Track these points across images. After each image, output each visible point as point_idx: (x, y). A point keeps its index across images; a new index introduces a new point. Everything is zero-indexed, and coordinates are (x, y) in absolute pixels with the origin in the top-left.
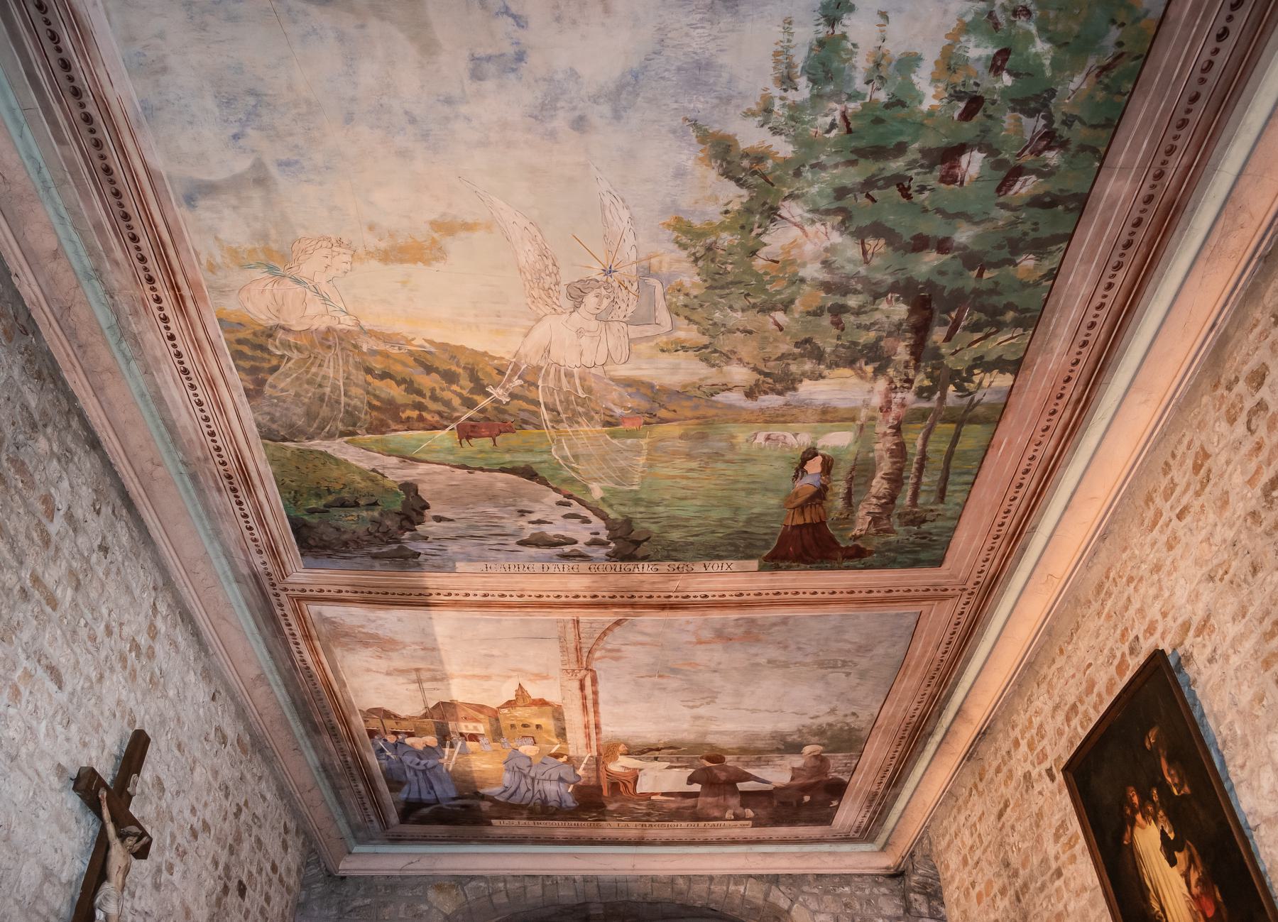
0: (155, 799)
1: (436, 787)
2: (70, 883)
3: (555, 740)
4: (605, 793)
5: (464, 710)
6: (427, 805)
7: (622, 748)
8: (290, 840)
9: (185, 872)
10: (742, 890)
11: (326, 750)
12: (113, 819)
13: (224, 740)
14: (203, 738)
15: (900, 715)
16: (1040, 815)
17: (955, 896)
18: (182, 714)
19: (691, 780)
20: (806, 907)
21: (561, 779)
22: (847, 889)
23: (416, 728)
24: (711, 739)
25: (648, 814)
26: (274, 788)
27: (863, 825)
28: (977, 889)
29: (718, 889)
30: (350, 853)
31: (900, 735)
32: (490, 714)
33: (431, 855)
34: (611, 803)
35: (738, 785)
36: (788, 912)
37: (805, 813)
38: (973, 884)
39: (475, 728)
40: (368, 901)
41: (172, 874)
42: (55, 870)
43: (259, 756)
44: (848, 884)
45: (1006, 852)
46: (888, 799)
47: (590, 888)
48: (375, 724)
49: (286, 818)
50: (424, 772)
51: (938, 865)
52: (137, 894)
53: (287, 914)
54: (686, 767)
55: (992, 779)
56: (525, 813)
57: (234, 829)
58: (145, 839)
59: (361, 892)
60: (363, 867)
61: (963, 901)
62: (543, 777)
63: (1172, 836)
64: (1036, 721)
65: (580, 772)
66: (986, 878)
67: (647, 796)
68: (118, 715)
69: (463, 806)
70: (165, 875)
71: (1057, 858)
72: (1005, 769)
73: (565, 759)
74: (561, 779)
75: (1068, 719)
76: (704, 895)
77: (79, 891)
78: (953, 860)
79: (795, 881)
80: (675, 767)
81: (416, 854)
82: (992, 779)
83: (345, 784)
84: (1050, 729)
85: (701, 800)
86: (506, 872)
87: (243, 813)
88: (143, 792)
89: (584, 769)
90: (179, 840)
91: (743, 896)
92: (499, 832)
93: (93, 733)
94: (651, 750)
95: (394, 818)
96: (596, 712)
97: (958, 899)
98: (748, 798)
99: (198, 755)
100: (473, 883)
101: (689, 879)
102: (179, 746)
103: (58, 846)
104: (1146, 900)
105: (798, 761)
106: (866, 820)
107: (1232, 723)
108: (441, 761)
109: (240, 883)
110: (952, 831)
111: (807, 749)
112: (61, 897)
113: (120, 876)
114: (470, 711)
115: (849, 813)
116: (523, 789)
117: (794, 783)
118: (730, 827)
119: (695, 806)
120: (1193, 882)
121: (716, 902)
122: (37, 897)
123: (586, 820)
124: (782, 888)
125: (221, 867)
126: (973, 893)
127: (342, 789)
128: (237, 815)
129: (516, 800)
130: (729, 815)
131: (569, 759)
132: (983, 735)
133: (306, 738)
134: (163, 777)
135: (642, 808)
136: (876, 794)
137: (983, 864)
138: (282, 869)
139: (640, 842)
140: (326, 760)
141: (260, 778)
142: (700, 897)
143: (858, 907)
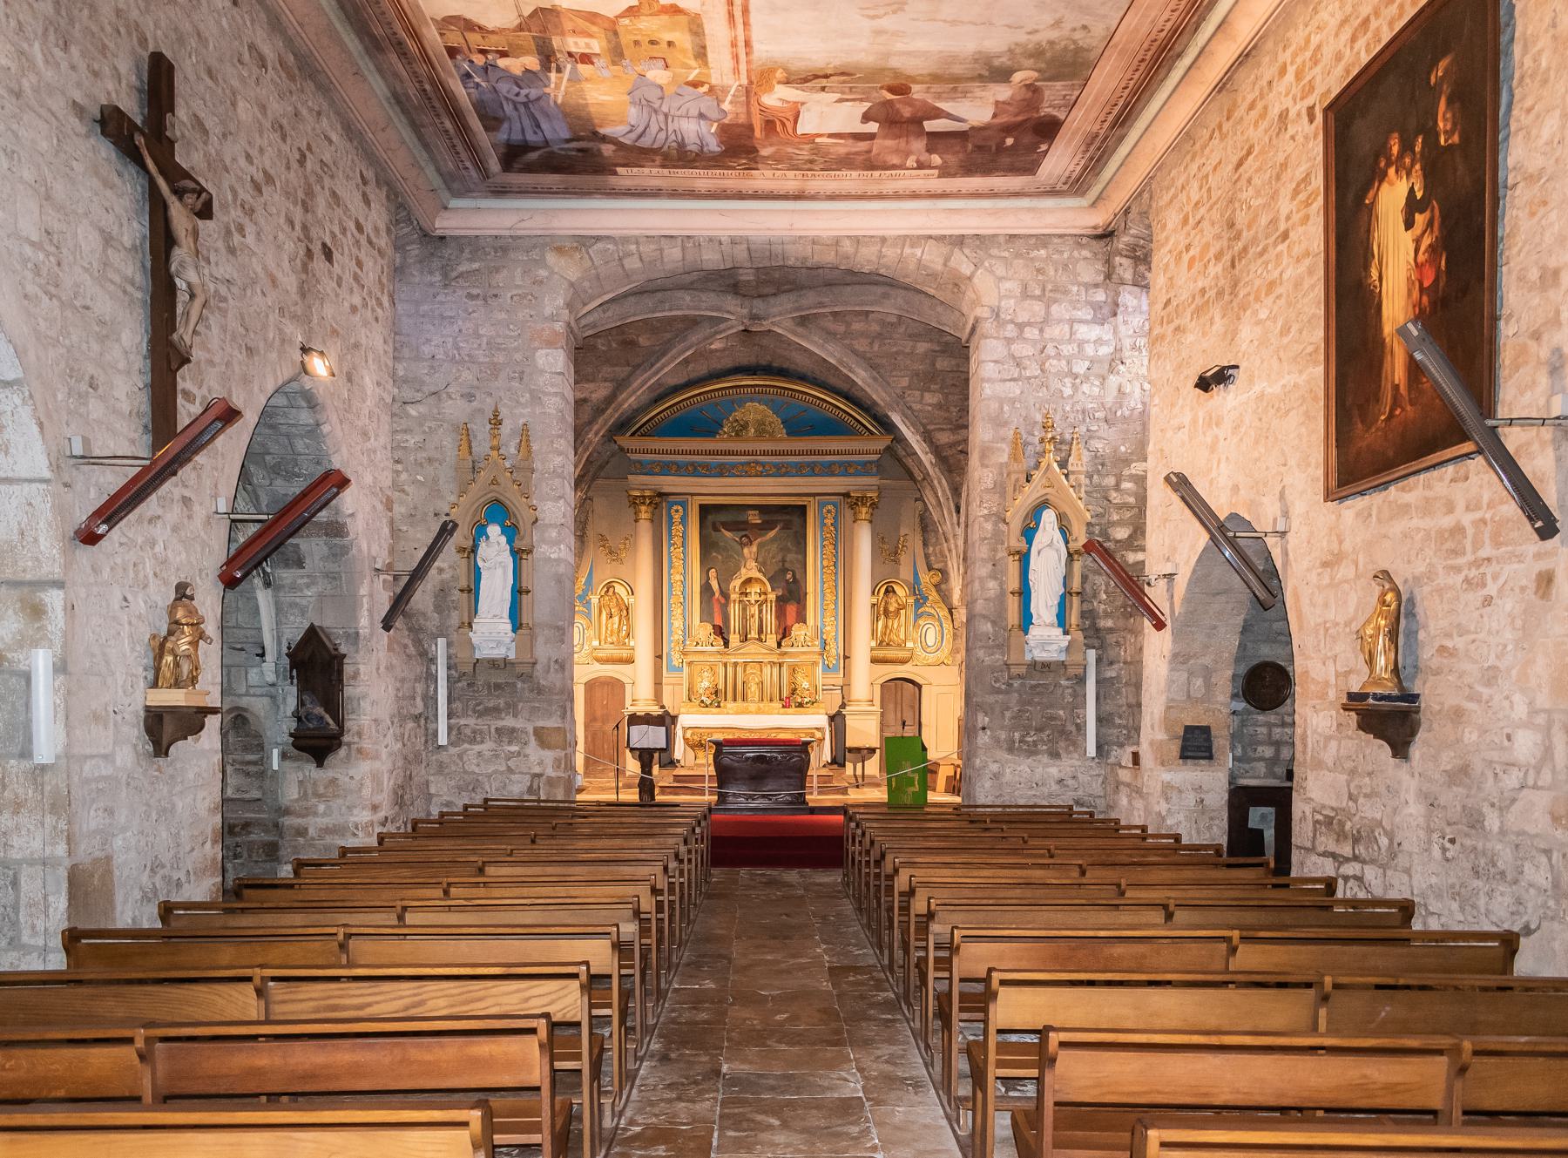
0: (200, 145)
1: (544, 126)
2: (134, 247)
3: (693, 63)
4: (758, 133)
5: (571, 19)
6: (534, 149)
7: (780, 74)
8: (370, 189)
9: (258, 234)
10: (919, 254)
11: (396, 75)
12: (162, 172)
13: (262, 63)
14: (235, 61)
15: (1145, 30)
16: (1284, 166)
17: (1165, 261)
18: (202, 27)
19: (866, 118)
20: (992, 272)
21: (701, 116)
22: (1043, 252)
23: (510, 45)
24: (895, 63)
25: (811, 162)
26: (339, 127)
27: (1074, 176)
28: (1192, 253)
29: (891, 253)
30: (446, 208)
31: (1139, 57)
32: (606, 25)
33: (545, 211)
34: (764, 147)
35: (926, 123)
36: (970, 278)
37: (1005, 160)
38: (1188, 248)
39: (588, 45)
40: (476, 266)
41: (244, 236)
42: (114, 233)
43: (311, 84)
44: (1045, 246)
45: (1234, 211)
46: (1110, 142)
47: (741, 254)
48: (455, 39)
49: (362, 166)
50: (525, 105)
51: (1154, 224)
52: (212, 259)
53: (385, 281)
54: (861, 100)
55: (1242, 118)
56: (658, 159)
57: (303, 181)
58: (204, 195)
59: (466, 254)
60: (464, 226)
61: (1172, 266)
62: (679, 113)
63: (1419, 195)
64: (1315, 40)
65: (726, 106)
66: (1204, 240)
67: (810, 139)
68: (122, 30)
69: (579, 150)
70: (237, 238)
71: (1288, 218)
72: (1260, 105)
73: (705, 88)
74: (701, 116)
75: (1354, 39)
76: (874, 258)
77: (148, 257)
78: (1172, 218)
79: (982, 241)
80: (847, 100)
81: (528, 210)
82: (1242, 118)
83: (426, 120)
84: (1328, 53)
85: (877, 144)
86: (637, 233)
87: (308, 161)
88: (183, 136)
89: (731, 102)
90: (242, 195)
91: (920, 260)
92: (627, 183)
93: (100, 57)
94: (816, 77)
95: (494, 165)
96: (746, 24)
97: (1167, 265)
98: (936, 140)
99: (235, 83)
100: (600, 245)
101: (857, 240)
102: (210, 72)
103: (107, 204)
104: (1367, 267)
105: (1003, 92)
106: (1079, 168)
107: (1540, 52)
108: (547, 90)
109: (324, 245)
110: (1179, 183)
111: (1018, 77)
112: (130, 263)
113: (191, 240)
114: (580, 22)
115: (1059, 160)
116: (654, 128)
117: (996, 121)
118: (912, 178)
119: (869, 151)
120: (1423, 248)
121: (888, 268)
122: (105, 264)
123: (734, 168)
124: (967, 251)
125: (298, 227)
126: (1186, 258)
127: (423, 126)
128: (302, 161)
129: (645, 142)
130: (911, 162)
131: (712, 89)
132: (1245, 57)
133: (367, 58)
134: (202, 115)
135: (805, 153)
136: (1097, 135)
137: (1205, 224)
138: (368, 228)
139: (799, 197)
140: (398, 88)
141: (319, 113)
142: (869, 261)
143: (1052, 273)
